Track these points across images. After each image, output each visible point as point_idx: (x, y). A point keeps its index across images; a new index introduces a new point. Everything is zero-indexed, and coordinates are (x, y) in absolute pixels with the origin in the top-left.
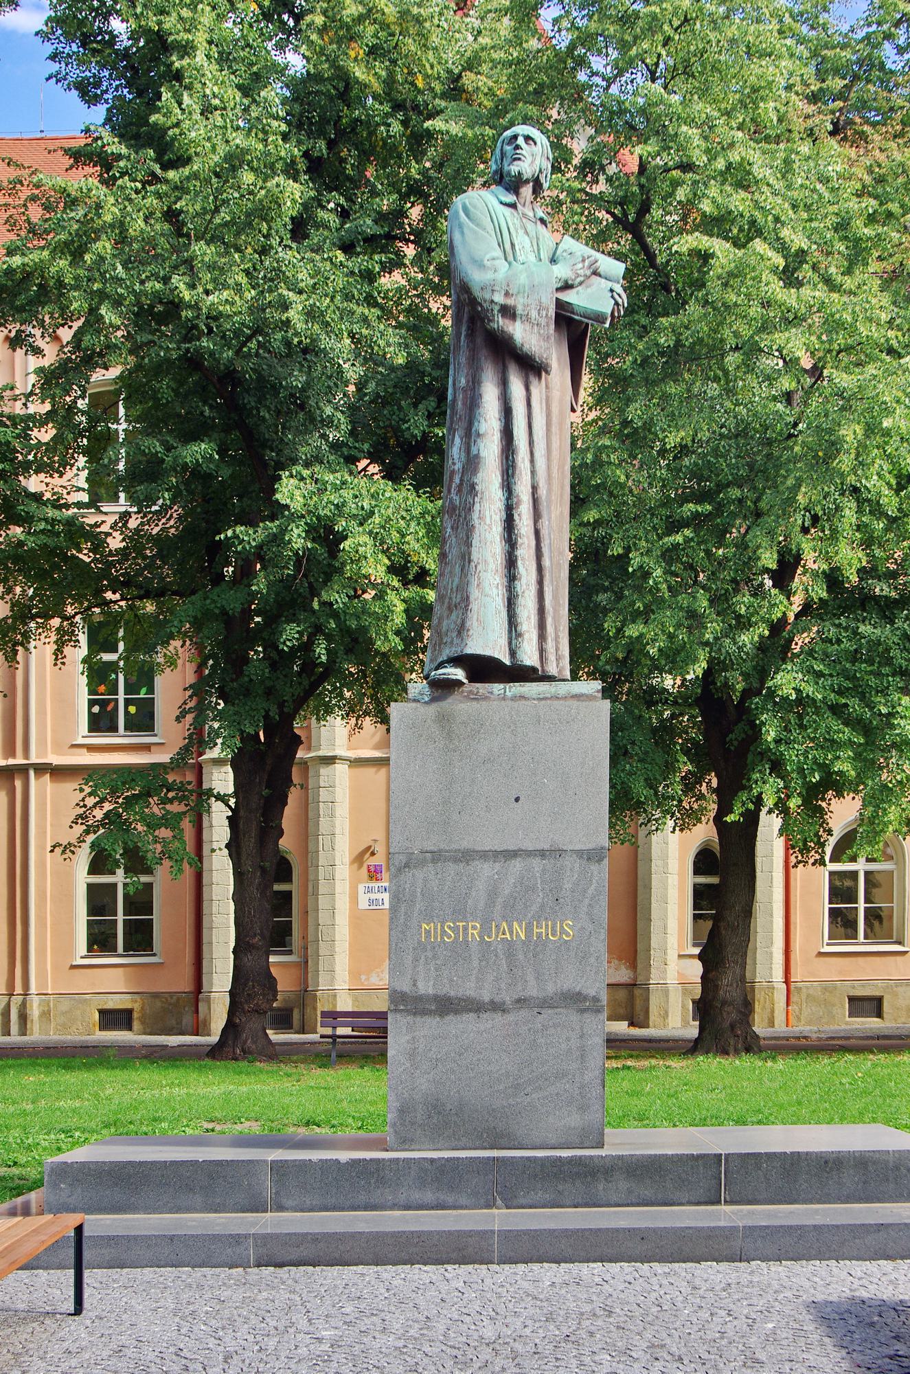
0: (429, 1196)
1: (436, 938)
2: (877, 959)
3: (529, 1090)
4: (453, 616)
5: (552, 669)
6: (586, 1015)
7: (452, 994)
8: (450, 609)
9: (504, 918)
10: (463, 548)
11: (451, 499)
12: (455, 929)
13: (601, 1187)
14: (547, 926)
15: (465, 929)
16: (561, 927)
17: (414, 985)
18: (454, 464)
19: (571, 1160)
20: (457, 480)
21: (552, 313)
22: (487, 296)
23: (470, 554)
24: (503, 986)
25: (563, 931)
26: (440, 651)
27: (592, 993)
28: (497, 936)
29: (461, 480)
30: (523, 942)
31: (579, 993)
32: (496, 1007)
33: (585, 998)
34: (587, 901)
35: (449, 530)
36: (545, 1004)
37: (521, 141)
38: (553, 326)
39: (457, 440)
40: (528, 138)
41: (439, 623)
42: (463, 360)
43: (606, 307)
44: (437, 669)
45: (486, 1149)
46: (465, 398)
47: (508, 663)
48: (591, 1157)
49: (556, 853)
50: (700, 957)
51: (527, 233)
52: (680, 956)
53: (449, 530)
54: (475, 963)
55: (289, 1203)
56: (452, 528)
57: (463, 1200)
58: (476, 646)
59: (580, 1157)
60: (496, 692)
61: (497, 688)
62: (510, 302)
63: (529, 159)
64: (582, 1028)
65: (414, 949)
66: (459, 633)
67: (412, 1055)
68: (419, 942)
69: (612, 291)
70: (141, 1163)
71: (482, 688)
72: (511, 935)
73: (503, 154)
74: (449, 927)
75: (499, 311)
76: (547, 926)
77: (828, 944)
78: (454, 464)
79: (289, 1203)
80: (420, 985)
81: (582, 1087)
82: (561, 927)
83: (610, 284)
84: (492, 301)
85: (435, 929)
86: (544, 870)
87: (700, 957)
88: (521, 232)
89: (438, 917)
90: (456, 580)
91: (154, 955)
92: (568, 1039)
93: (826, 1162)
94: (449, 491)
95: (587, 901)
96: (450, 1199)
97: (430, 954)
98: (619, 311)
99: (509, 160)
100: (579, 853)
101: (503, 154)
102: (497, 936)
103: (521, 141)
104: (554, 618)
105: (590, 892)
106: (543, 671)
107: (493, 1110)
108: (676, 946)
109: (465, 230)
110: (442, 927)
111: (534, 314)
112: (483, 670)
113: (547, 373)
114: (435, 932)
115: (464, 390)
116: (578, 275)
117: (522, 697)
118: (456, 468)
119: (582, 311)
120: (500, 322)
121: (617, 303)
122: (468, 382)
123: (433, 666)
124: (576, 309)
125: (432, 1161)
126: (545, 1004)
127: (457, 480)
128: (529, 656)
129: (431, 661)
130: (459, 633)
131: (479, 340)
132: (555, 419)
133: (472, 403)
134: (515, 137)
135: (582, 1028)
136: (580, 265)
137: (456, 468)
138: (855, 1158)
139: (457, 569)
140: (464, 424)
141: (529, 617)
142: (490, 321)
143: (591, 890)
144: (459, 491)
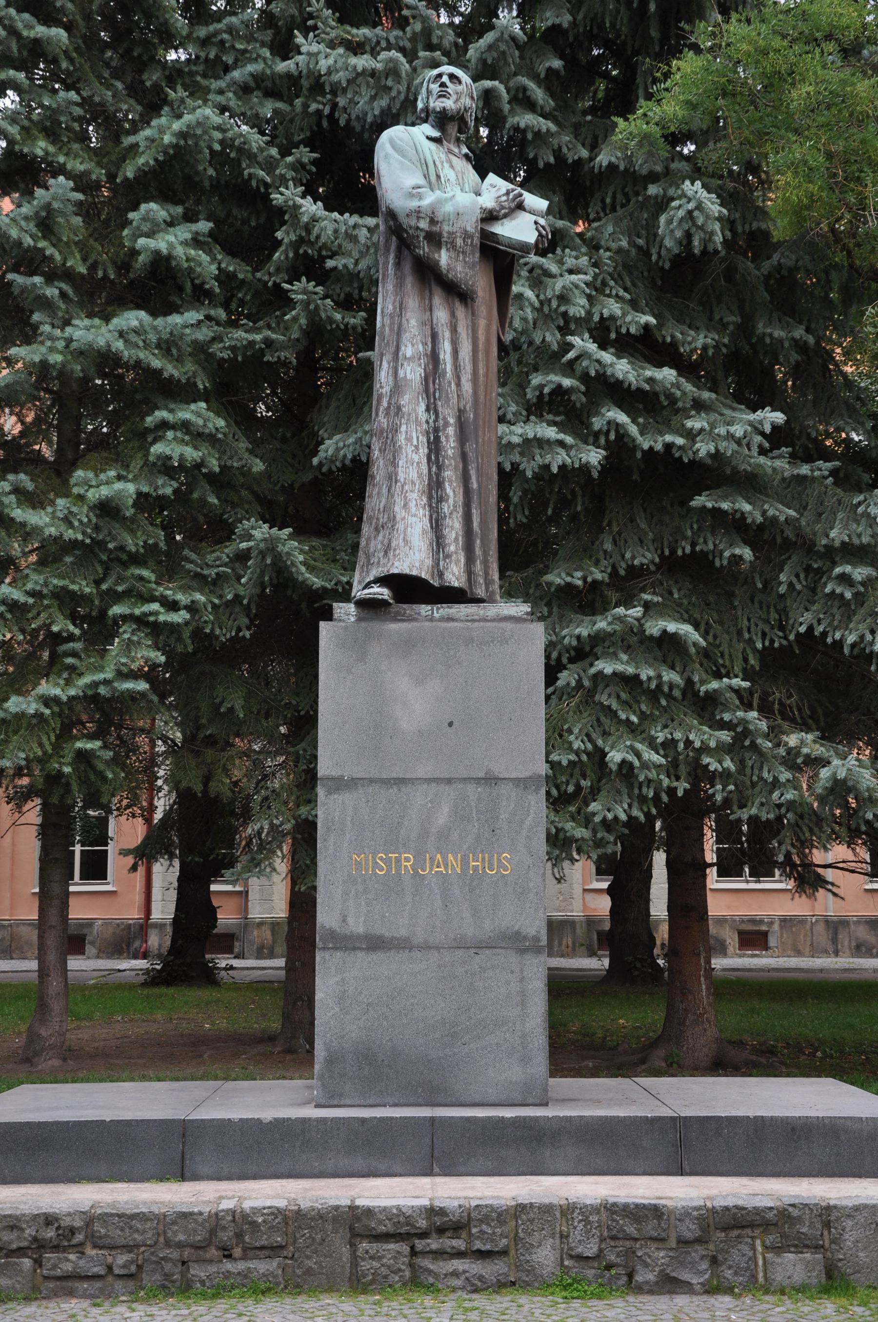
0: (360, 1163)
1: (367, 870)
2: (761, 895)
3: (466, 1038)
4: (380, 537)
5: (481, 592)
6: (527, 956)
7: (386, 934)
8: (377, 530)
9: (439, 850)
10: (391, 469)
11: (379, 422)
12: (387, 861)
13: (548, 1154)
14: (483, 859)
15: (398, 860)
16: (499, 860)
17: (344, 921)
18: (381, 387)
19: (515, 1121)
20: (385, 404)
21: (477, 241)
22: (413, 222)
23: (396, 474)
24: (438, 923)
25: (501, 865)
26: (368, 572)
27: (532, 932)
28: (431, 869)
29: (389, 403)
30: (459, 876)
31: (518, 933)
32: (427, 947)
33: (525, 938)
34: (524, 833)
35: (377, 452)
36: (480, 946)
37: (445, 79)
38: (478, 255)
39: (385, 365)
40: (452, 77)
41: (368, 544)
42: (390, 287)
43: (531, 237)
44: (364, 589)
45: (420, 1105)
46: (392, 324)
47: (436, 584)
48: (536, 1119)
49: (491, 780)
50: (610, 891)
51: (452, 166)
52: (585, 890)
53: (377, 452)
54: (408, 898)
55: (204, 1170)
56: (380, 450)
57: (397, 1168)
58: (401, 566)
59: (525, 1118)
60: (423, 613)
61: (424, 609)
62: (436, 229)
63: (454, 97)
64: (522, 971)
65: (344, 882)
66: (386, 553)
67: (341, 998)
68: (350, 875)
69: (536, 223)
70: (40, 1124)
71: (408, 609)
72: (446, 868)
73: (429, 93)
74: (381, 859)
75: (425, 238)
76: (483, 859)
77: (717, 881)
78: (381, 387)
79: (204, 1170)
80: (350, 921)
81: (523, 1036)
82: (499, 860)
83: (534, 218)
84: (418, 228)
85: (366, 859)
86: (479, 800)
87: (610, 891)
88: (446, 165)
89: (369, 847)
90: (384, 500)
91: (108, 884)
92: (507, 983)
93: (793, 1129)
94: (377, 414)
95: (524, 833)
96: (383, 1167)
97: (360, 888)
98: (543, 242)
99: (435, 96)
100: (516, 781)
101: (429, 93)
102: (431, 869)
103: (445, 79)
104: (482, 541)
105: (527, 823)
106: (472, 592)
107: (428, 1061)
108: (580, 881)
109: (391, 161)
110: (374, 858)
111: (459, 242)
112: (409, 590)
113: (473, 300)
114: (367, 864)
115: (391, 316)
116: (503, 208)
117: (450, 619)
118: (384, 391)
119: (506, 242)
120: (424, 249)
121: (540, 235)
122: (395, 308)
123: (360, 588)
124: (501, 239)
125: (363, 1121)
126: (480, 946)
127: (385, 404)
128: (455, 576)
129: (360, 582)
130: (386, 553)
131: (407, 267)
132: (481, 346)
133: (399, 328)
134: (440, 76)
135: (522, 971)
136: (504, 198)
137: (384, 391)
138: (824, 1125)
139: (385, 490)
140: (392, 349)
141: (456, 539)
142: (415, 247)
143: (529, 821)
144: (387, 414)
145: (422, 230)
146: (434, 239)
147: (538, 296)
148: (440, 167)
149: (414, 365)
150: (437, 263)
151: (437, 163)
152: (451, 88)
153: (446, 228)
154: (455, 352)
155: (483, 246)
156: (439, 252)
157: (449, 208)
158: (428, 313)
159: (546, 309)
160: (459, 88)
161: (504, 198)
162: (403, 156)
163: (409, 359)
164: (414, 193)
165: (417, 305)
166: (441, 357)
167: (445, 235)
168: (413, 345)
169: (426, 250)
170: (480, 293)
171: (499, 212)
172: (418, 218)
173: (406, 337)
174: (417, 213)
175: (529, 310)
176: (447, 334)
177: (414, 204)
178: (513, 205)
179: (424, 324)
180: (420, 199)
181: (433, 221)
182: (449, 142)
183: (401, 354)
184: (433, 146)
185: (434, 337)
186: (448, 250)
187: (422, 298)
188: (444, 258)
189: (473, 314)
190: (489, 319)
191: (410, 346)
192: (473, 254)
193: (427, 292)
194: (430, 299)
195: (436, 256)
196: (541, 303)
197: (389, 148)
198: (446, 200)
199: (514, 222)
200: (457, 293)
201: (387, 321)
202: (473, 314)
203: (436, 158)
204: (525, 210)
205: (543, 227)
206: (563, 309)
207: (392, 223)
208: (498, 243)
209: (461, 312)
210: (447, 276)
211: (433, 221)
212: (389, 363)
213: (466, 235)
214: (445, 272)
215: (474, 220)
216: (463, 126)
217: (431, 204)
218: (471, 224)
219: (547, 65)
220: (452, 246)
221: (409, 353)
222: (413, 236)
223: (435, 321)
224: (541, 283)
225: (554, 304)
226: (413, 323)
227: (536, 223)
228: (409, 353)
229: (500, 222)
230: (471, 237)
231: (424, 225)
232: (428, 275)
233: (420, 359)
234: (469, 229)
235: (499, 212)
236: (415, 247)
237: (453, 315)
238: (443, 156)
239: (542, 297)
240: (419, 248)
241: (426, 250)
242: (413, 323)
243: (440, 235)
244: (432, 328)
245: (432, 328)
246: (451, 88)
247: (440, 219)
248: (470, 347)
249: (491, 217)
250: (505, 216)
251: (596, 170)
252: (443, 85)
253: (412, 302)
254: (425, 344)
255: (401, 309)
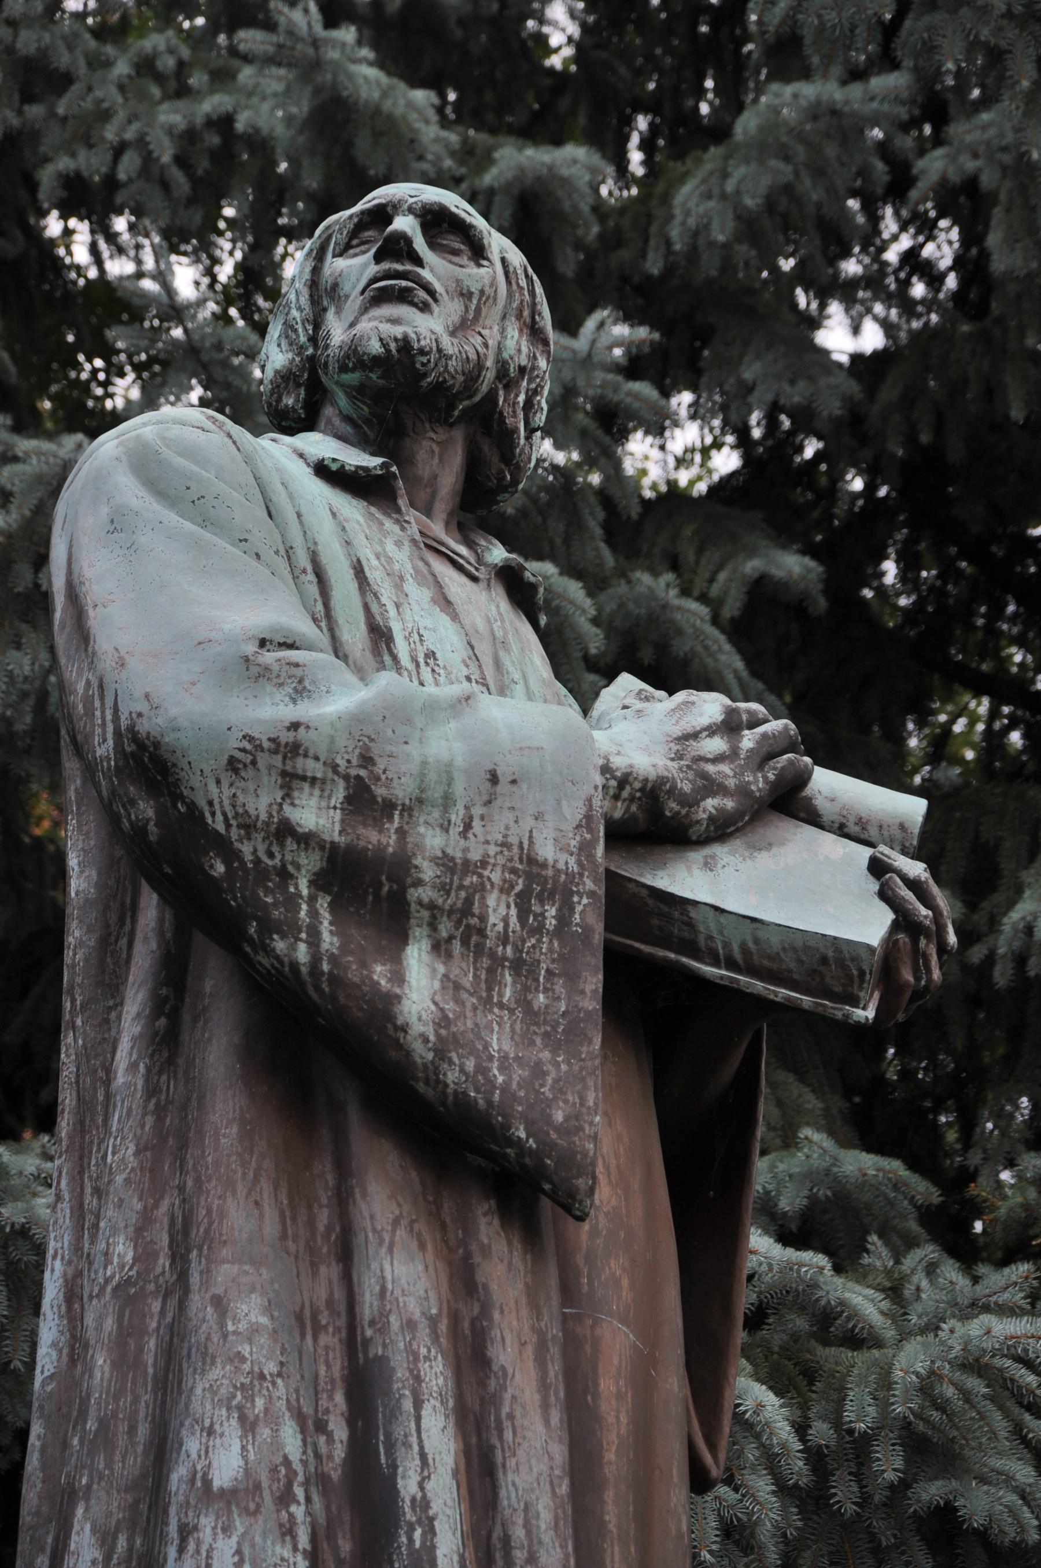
22: (261, 801)
38: (593, 982)
51: (445, 602)
62: (381, 838)
84: (285, 831)
88: (419, 595)
98: (918, 957)
99: (355, 302)
111: (498, 911)
113: (572, 1205)
115: (128, 1295)
116: (711, 786)
119: (736, 939)
120: (315, 936)
122: (145, 1256)
131: (217, 1048)
132: (613, 1457)
140: (128, 1463)
142: (268, 927)
145: (306, 840)
146: (371, 889)
147: (801, 1429)
148: (387, 596)
149: (258, 1528)
150: (384, 1008)
151: (374, 573)
152: (436, 268)
153: (431, 840)
154: (481, 1471)
155: (617, 964)
156: (395, 958)
157: (443, 745)
158: (329, 1271)
159: (844, 1494)
160: (476, 275)
161: (716, 745)
162: (205, 522)
163: (229, 1497)
164: (265, 663)
165: (271, 1227)
166: (408, 1486)
167: (429, 872)
168: (248, 1426)
169: (329, 940)
170: (605, 1196)
171: (691, 802)
172: (290, 781)
173: (207, 1387)
174: (287, 756)
175: (763, 1486)
176: (436, 1374)
177: (268, 712)
178: (759, 783)
179: (304, 1322)
180: (301, 691)
181: (363, 800)
182: (428, 512)
183: (177, 1477)
184: (352, 509)
185: (365, 1386)
186: (439, 948)
187: (298, 1197)
188: (419, 985)
189: (568, 1292)
190: (647, 1329)
191: (231, 1429)
192: (572, 977)
193: (325, 1170)
194: (343, 1201)
195: (380, 973)
196: (816, 1457)
197: (130, 491)
198: (432, 709)
199: (764, 860)
200: (483, 1167)
201: (101, 1319)
202: (568, 1292)
203: (367, 553)
204: (813, 818)
205: (914, 885)
206: (931, 1491)
207: (146, 809)
208: (691, 948)
209: (503, 1268)
210: (433, 1075)
211: (363, 800)
212: (106, 1540)
213: (534, 882)
214: (422, 1054)
215: (574, 812)
216: (489, 434)
217: (357, 719)
218: (558, 834)
219: (752, 566)
220: (461, 930)
221: (227, 1465)
222: (261, 872)
223: (368, 1304)
224: (810, 1375)
225: (889, 1464)
226: (246, 1312)
227: (877, 868)
228: (227, 1465)
229: (696, 856)
230: (563, 893)
231: (315, 814)
232: (332, 1073)
233: (285, 1498)
234: (547, 851)
235: (691, 802)
236: (268, 927)
237: (464, 1280)
238: (402, 557)
239: (821, 1432)
240: (290, 929)
241: (329, 940)
242: (246, 1312)
243: (400, 868)
244: (353, 1343)
245: (353, 1343)
246: (436, 268)
247: (403, 790)
248: (559, 1452)
249: (649, 820)
250: (722, 830)
251: (1002, 976)
252: (396, 248)
253: (244, 1212)
254: (312, 1426)
255: (179, 1257)
